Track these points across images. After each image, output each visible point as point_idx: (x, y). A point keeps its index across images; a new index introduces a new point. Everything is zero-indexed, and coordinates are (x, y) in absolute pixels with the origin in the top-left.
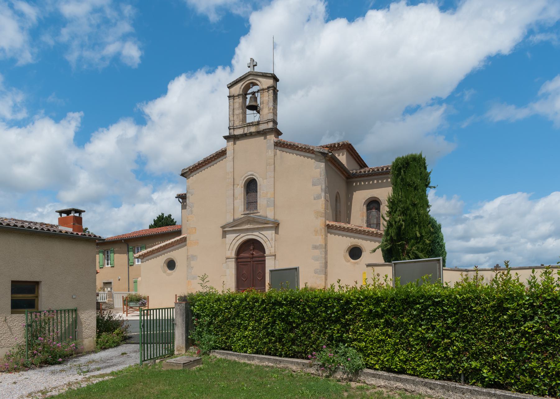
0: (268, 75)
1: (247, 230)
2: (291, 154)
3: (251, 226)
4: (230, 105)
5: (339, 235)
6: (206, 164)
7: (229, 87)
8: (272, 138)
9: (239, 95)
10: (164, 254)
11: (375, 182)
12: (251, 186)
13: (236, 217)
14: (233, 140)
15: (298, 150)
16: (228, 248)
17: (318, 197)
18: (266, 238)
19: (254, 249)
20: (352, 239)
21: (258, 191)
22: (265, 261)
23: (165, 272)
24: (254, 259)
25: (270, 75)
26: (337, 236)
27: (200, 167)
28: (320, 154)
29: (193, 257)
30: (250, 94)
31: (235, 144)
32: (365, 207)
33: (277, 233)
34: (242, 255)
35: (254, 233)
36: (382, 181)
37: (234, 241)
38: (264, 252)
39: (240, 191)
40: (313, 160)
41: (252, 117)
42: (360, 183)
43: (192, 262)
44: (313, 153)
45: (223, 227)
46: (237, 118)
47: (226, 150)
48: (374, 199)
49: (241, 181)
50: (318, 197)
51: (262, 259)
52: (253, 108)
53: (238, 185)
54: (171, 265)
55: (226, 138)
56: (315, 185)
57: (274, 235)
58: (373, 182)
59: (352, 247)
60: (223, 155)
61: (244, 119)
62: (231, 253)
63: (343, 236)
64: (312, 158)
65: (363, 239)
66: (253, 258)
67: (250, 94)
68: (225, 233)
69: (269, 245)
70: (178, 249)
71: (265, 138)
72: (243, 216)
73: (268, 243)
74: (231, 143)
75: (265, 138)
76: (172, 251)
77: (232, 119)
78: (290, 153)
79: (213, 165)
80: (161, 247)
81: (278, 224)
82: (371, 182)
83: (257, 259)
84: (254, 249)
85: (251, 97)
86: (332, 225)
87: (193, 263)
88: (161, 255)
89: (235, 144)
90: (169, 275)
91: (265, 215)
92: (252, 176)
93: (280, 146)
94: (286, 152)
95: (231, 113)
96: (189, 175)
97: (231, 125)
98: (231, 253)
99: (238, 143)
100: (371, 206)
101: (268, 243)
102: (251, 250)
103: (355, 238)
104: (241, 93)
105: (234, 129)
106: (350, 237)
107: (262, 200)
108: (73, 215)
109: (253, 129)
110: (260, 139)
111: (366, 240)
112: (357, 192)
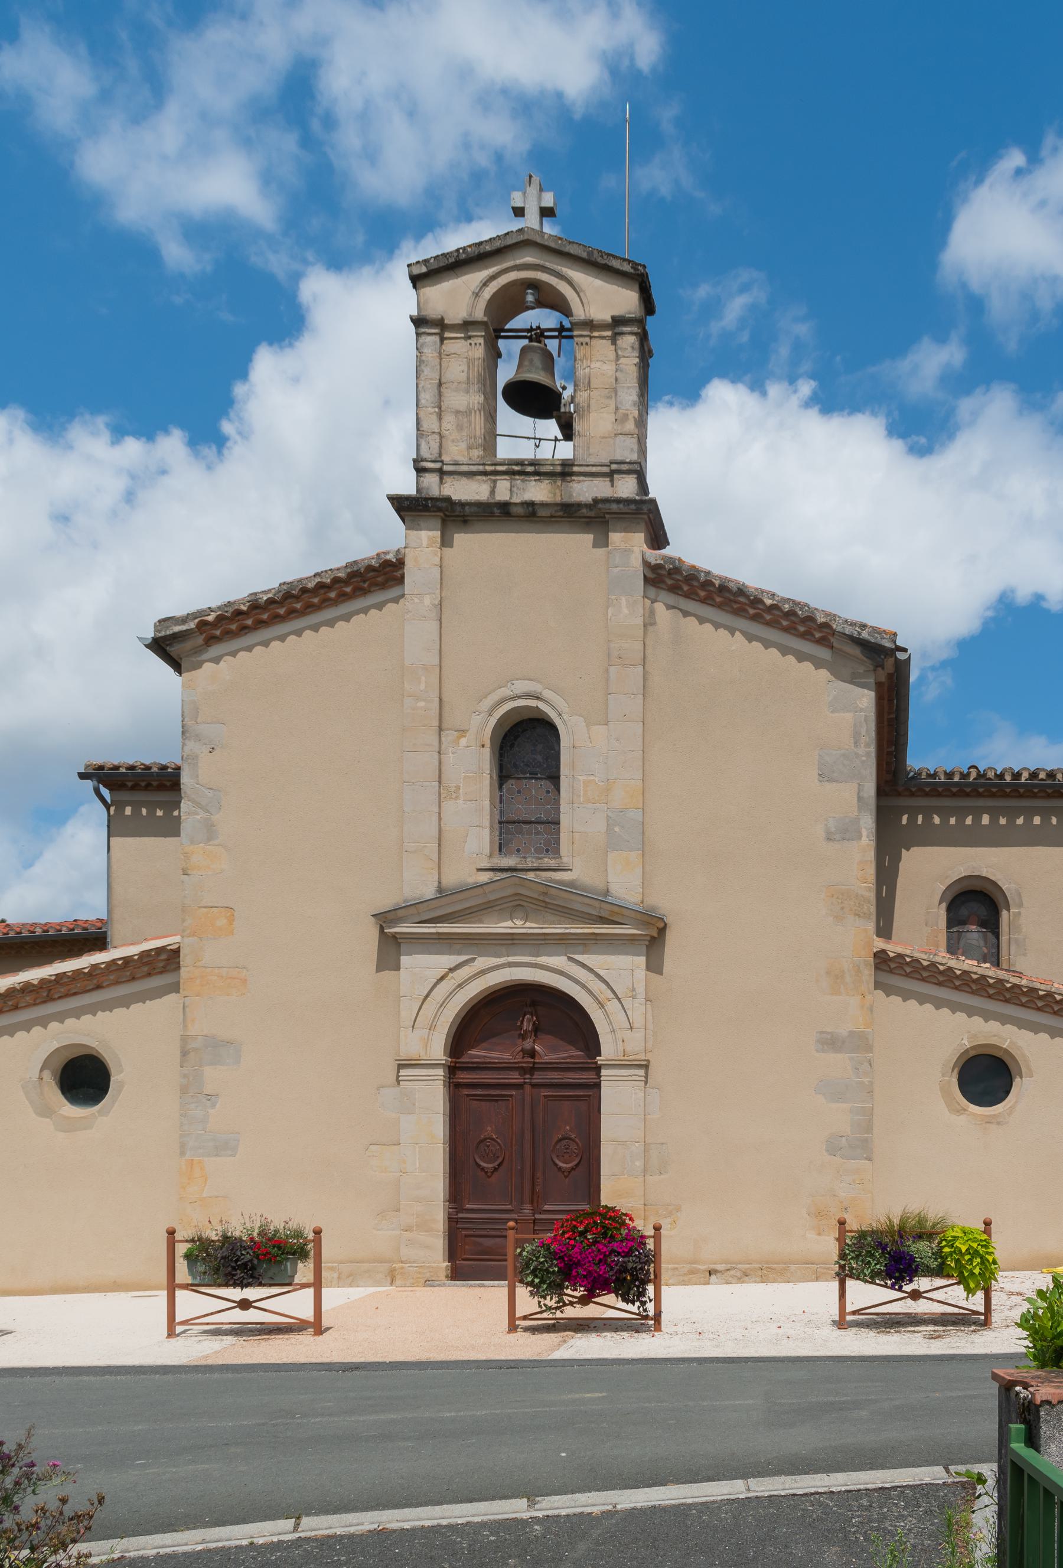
0: (615, 264)
1: (510, 942)
2: (723, 633)
3: (531, 927)
4: (420, 363)
5: (922, 999)
6: (292, 614)
7: (416, 280)
8: (631, 545)
9: (467, 326)
10: (43, 1022)
11: (986, 819)
12: (526, 746)
14: (438, 523)
15: (755, 618)
16: (407, 1012)
17: (845, 833)
18: (606, 984)
19: (536, 1030)
20: (977, 1020)
21: (564, 771)
22: (598, 1086)
23: (46, 1111)
24: (538, 1077)
25: (627, 268)
26: (913, 1003)
27: (260, 624)
28: (856, 651)
29: (219, 1048)
30: (516, 334)
31: (446, 542)
32: (941, 915)
33: (655, 966)
34: (477, 1054)
35: (543, 960)
36: (1011, 821)
37: (438, 987)
39: (472, 761)
40: (824, 674)
41: (523, 437)
42: (928, 819)
43: (208, 1072)
44: (823, 642)
45: (385, 919)
46: (460, 428)
47: (400, 563)
48: (977, 885)
49: (476, 720)
50: (845, 833)
51: (586, 1077)
52: (534, 399)
53: (462, 732)
54: (84, 1078)
55: (403, 506)
56: (832, 780)
57: (641, 973)
58: (977, 819)
59: (972, 1053)
60: (384, 586)
61: (491, 436)
62: (426, 1043)
63: (939, 1004)
64: (818, 664)
65: (1021, 1024)
66: (532, 1070)
67: (516, 334)
68: (391, 947)
69: (619, 1018)
70: (125, 1002)
71: (602, 542)
72: (484, 877)
73: (613, 1006)
74: (427, 536)
75: (602, 542)
76: (92, 1009)
77: (431, 423)
78: (717, 626)
79: (331, 623)
80: (27, 988)
81: (662, 931)
82: (969, 821)
83: (555, 1076)
84: (536, 1030)
85: (524, 350)
86: (94, 967)
87: (213, 1076)
88: (27, 1026)
89: (446, 542)
90: (69, 1126)
91: (600, 884)
92: (533, 703)
93: (674, 589)
94: (702, 620)
95: (427, 397)
96: (198, 651)
97: (425, 453)
98: (426, 1043)
99: (462, 539)
100: (964, 912)
101: (613, 1006)
102: (523, 1037)
103: (987, 1016)
104: (479, 314)
105: (442, 473)
106: (971, 1012)
109: (538, 492)
110: (576, 544)
111: (1036, 1028)
112: (915, 850)
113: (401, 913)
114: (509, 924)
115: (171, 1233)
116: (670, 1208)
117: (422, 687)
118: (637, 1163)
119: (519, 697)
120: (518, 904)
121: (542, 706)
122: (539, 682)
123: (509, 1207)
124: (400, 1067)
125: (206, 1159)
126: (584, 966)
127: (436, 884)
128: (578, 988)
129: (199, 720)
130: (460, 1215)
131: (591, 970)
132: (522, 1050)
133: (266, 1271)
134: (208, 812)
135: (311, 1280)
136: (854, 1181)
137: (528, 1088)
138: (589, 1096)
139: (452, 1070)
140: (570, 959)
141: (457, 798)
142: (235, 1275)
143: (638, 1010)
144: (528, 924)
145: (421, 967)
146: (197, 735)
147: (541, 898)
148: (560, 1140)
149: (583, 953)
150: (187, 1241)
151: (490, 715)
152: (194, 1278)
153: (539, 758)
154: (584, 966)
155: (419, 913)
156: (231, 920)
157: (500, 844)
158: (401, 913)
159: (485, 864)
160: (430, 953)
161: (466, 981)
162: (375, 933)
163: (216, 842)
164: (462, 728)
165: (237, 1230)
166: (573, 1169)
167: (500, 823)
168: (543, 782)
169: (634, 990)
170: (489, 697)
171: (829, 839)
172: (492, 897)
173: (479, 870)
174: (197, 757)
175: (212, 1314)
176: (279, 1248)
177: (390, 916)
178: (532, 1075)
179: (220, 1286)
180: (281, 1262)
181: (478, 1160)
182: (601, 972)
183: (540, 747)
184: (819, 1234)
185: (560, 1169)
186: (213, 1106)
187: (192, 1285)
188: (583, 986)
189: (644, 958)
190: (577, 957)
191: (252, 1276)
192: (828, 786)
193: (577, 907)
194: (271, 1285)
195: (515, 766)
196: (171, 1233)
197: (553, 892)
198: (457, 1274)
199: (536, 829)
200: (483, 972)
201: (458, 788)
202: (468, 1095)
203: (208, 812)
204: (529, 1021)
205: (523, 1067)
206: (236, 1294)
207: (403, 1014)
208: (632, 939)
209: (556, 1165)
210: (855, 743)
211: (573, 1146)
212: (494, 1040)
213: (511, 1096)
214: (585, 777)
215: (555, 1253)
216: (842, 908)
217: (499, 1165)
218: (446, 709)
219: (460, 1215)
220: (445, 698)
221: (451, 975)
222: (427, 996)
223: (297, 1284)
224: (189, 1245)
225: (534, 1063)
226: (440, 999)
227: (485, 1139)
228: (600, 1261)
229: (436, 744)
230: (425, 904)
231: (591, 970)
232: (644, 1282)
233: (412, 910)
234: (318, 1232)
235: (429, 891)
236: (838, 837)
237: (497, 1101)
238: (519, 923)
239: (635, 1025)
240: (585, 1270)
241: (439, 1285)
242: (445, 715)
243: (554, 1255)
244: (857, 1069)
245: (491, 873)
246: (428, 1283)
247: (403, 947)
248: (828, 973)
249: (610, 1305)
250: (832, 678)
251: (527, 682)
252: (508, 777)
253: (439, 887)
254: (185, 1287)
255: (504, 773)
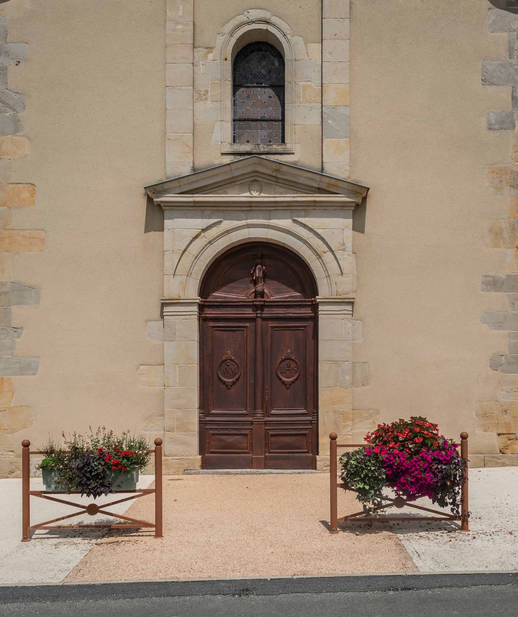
1: (249, 208)
12: (258, 61)
13: (202, 162)
16: (169, 264)
18: (322, 239)
19: (265, 276)
24: (267, 312)
34: (219, 295)
35: (274, 222)
37: (193, 242)
38: (315, 292)
39: (216, 69)
43: (15, 309)
49: (220, 40)
53: (210, 49)
57: (349, 233)
66: (262, 307)
68: (157, 208)
69: (333, 266)
72: (227, 160)
73: (328, 257)
80: (315, 202)
83: (280, 312)
84: (265, 276)
91: (316, 165)
92: (263, 27)
101: (328, 257)
107: (301, 116)
108: (403, 522)
113: (166, 186)
114: (248, 194)
115: (26, 445)
116: (371, 412)
117: (180, 13)
118: (347, 378)
119: (253, 22)
120: (254, 180)
121: (270, 28)
122: (268, 10)
123: (245, 412)
124: (163, 305)
125: (13, 377)
126: (305, 226)
127: (191, 165)
128: (301, 244)
129: (8, 40)
130: (208, 419)
131: (311, 230)
132: (255, 292)
133: (114, 479)
134: (15, 110)
135: (154, 488)
136: (511, 390)
137: (259, 321)
138: (305, 327)
139: (202, 307)
140: (295, 221)
141: (206, 99)
142: (89, 485)
143: (347, 261)
144: (262, 195)
145: (181, 228)
146: (6, 52)
147: (274, 174)
148: (283, 360)
149: (305, 217)
150: (41, 453)
151: (231, 36)
152: (49, 486)
153: (263, 72)
154: (305, 226)
155: (180, 186)
156: (32, 194)
157: (234, 137)
158: (166, 186)
159: (228, 149)
160: (187, 218)
161: (215, 239)
162: (143, 203)
163: (21, 133)
164: (210, 46)
165: (86, 443)
166: (293, 382)
167: (234, 120)
168: (266, 90)
169: (344, 245)
170: (231, 22)
171: (490, 129)
172: (236, 174)
173: (223, 154)
174: (6, 68)
175: (63, 518)
176: (128, 459)
177: (158, 188)
178: (262, 310)
179: (70, 492)
180: (129, 472)
181: (221, 376)
182: (319, 231)
183: (264, 63)
184: (485, 431)
185: (283, 382)
186: (19, 336)
187: (45, 492)
188: (305, 242)
189: (351, 221)
190: (300, 220)
191: (102, 485)
192: (490, 89)
193: (301, 180)
194: (117, 492)
195: (245, 77)
196: (26, 445)
197: (284, 169)
198: (206, 464)
199: (261, 125)
200: (228, 232)
201: (207, 91)
202: (213, 327)
203: (15, 110)
204: (260, 270)
205: (256, 305)
206: (87, 500)
207: (167, 264)
208: (343, 206)
209: (281, 379)
210: (510, 55)
211: (293, 365)
212: (231, 285)
213: (246, 327)
214: (304, 83)
215: (383, 462)
216: (501, 181)
217: (237, 380)
218: (198, 31)
219: (208, 419)
220: (196, 24)
221: (203, 234)
222: (185, 251)
223: (140, 491)
224: (43, 457)
225: (265, 302)
226: (195, 253)
227: (226, 360)
228: (425, 469)
229: (191, 57)
230: (186, 179)
231: (311, 230)
232: (454, 484)
233: (176, 184)
234: (464, 437)
235: (186, 170)
236: (497, 127)
237: (234, 331)
238: (255, 194)
239: (345, 272)
240: (413, 477)
241: (195, 473)
242: (197, 36)
243: (383, 464)
244: (513, 304)
245: (232, 157)
246: (186, 471)
247: (166, 213)
248: (490, 231)
249: (425, 505)
250: (492, 6)
251: (259, 10)
252: (241, 86)
253: (193, 167)
254: (39, 494)
255: (237, 83)
